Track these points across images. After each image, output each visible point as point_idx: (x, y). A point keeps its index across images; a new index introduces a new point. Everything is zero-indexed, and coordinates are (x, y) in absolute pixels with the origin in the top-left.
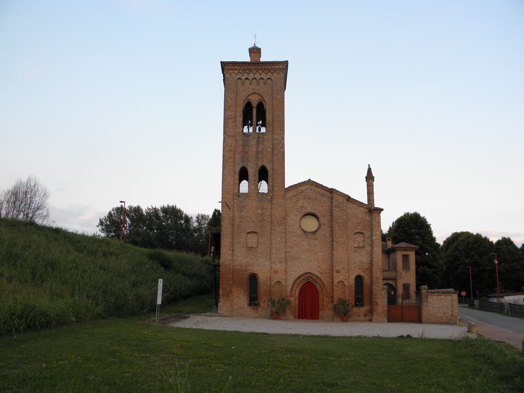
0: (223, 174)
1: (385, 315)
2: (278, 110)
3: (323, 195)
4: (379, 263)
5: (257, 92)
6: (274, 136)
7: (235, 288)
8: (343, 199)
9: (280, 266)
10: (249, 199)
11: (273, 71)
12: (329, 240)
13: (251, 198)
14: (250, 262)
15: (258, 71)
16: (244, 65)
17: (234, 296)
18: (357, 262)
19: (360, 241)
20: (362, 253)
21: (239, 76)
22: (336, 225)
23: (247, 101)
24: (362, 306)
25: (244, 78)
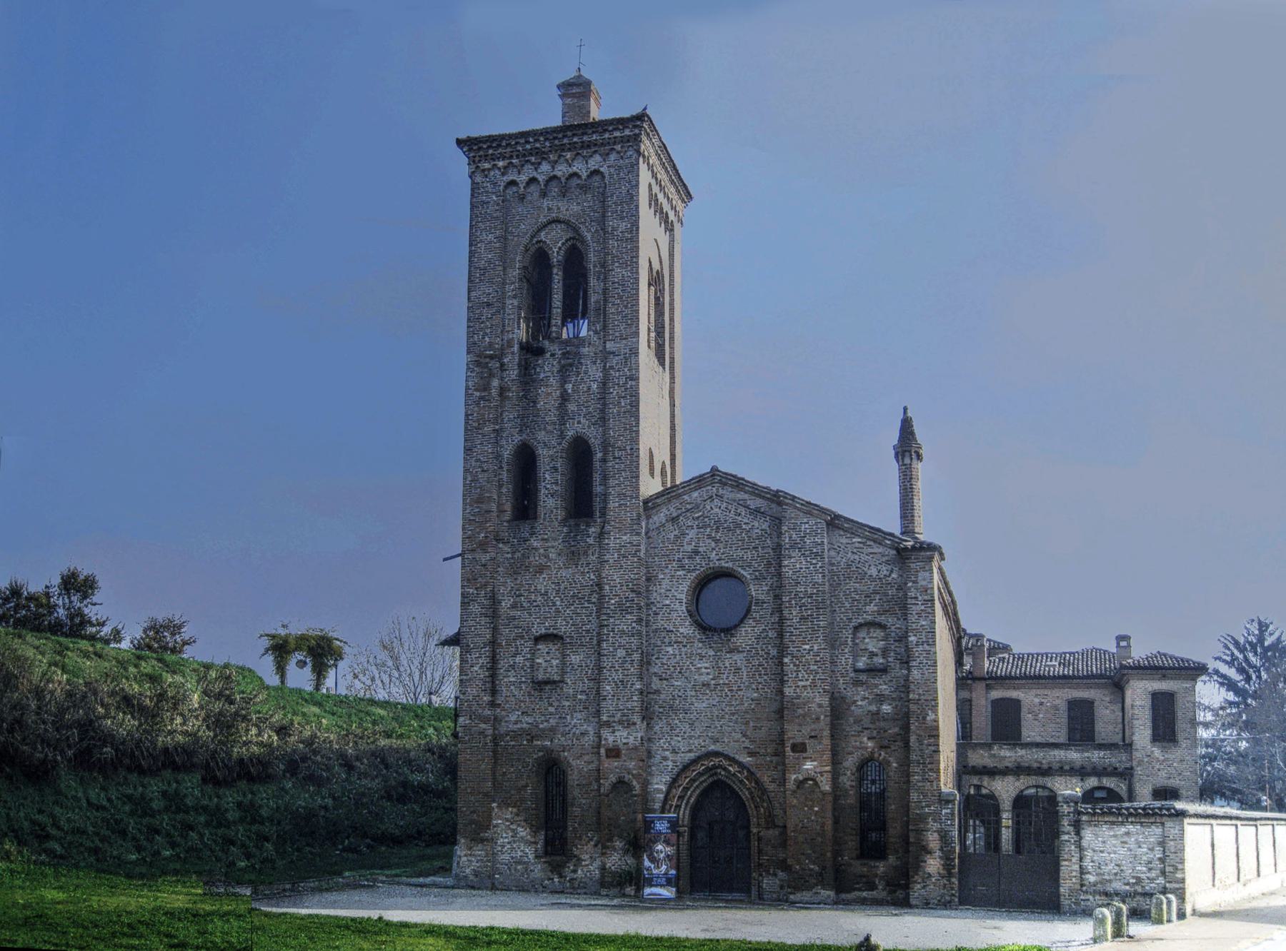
3: (757, 512)
6: (609, 345)
12: (775, 651)
14: (541, 726)
15: (564, 154)
19: (874, 650)
20: (880, 687)
23: (533, 249)
25: (523, 178)
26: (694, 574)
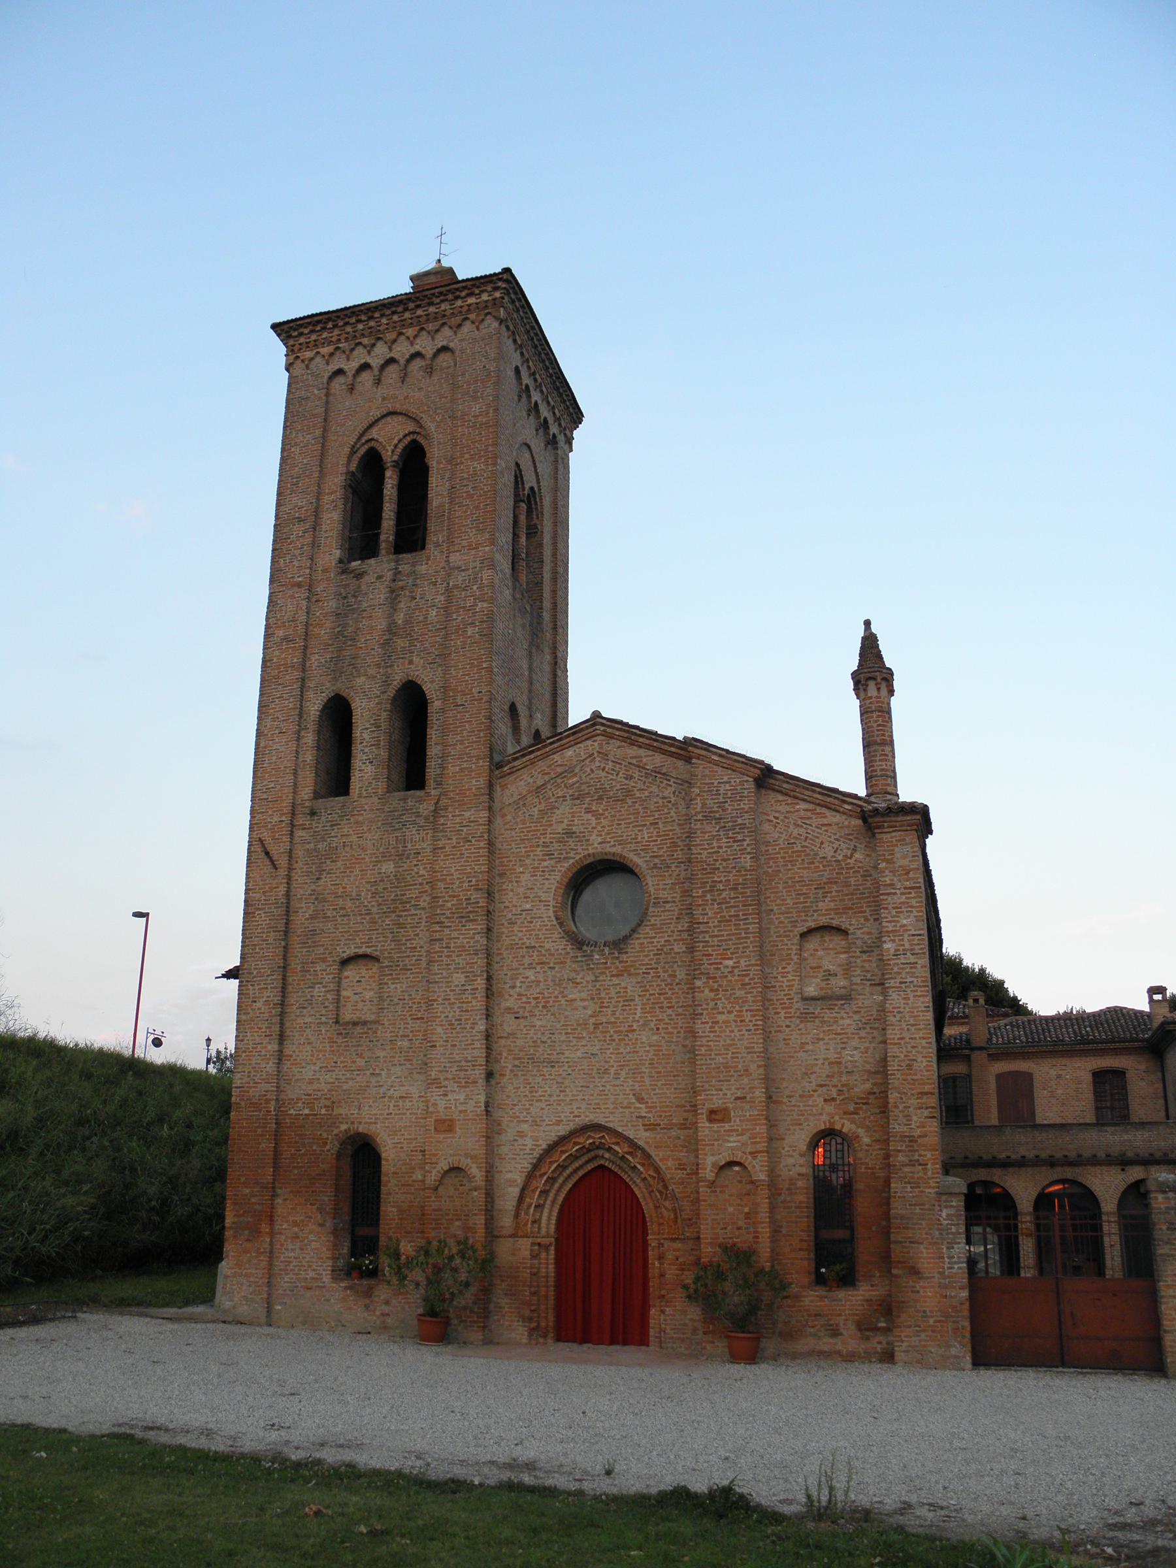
0: (259, 733)
1: (956, 1330)
2: (472, 458)
4: (915, 1066)
5: (398, 407)
7: (285, 1200)
8: (736, 779)
9: (462, 1097)
10: (352, 820)
11: (459, 319)
13: (361, 818)
14: (345, 1087)
15: (404, 331)
16: (353, 320)
17: (281, 1233)
18: (817, 1069)
20: (841, 1022)
21: (338, 362)
22: (709, 897)
24: (847, 1280)
26: (566, 865)
